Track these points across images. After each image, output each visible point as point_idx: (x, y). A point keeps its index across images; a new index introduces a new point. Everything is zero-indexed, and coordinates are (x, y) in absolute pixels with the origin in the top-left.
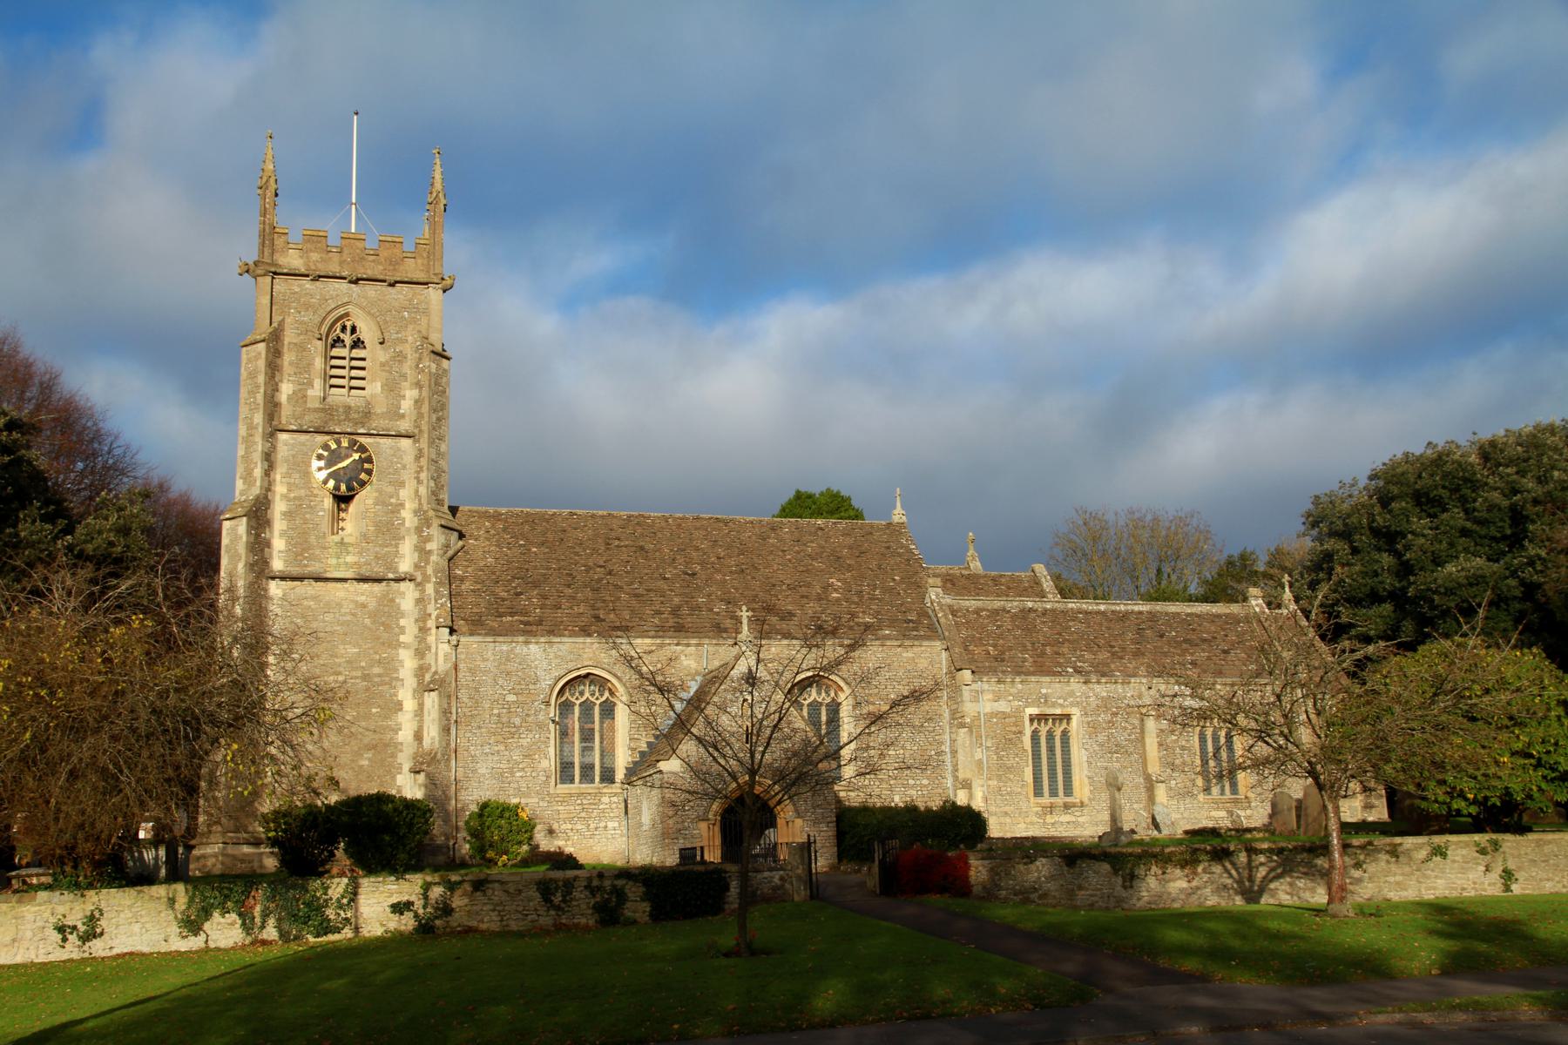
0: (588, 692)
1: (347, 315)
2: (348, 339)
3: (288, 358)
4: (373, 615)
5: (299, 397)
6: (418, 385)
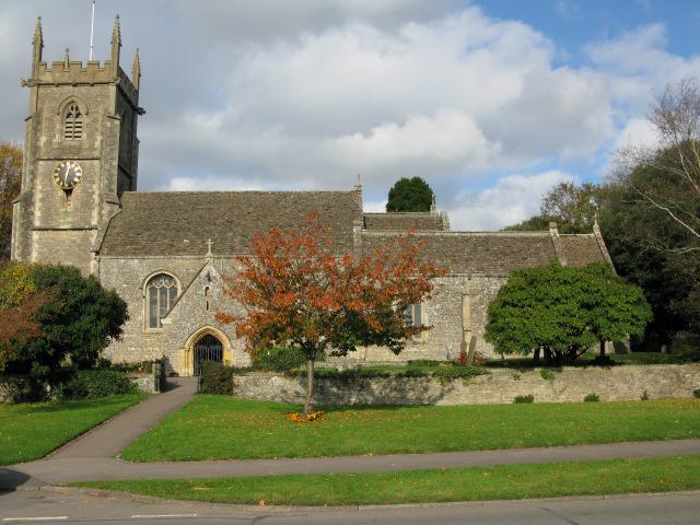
0: (164, 283)
1: (73, 102)
2: (74, 112)
3: (44, 124)
4: (79, 246)
5: (49, 143)
6: (102, 134)
